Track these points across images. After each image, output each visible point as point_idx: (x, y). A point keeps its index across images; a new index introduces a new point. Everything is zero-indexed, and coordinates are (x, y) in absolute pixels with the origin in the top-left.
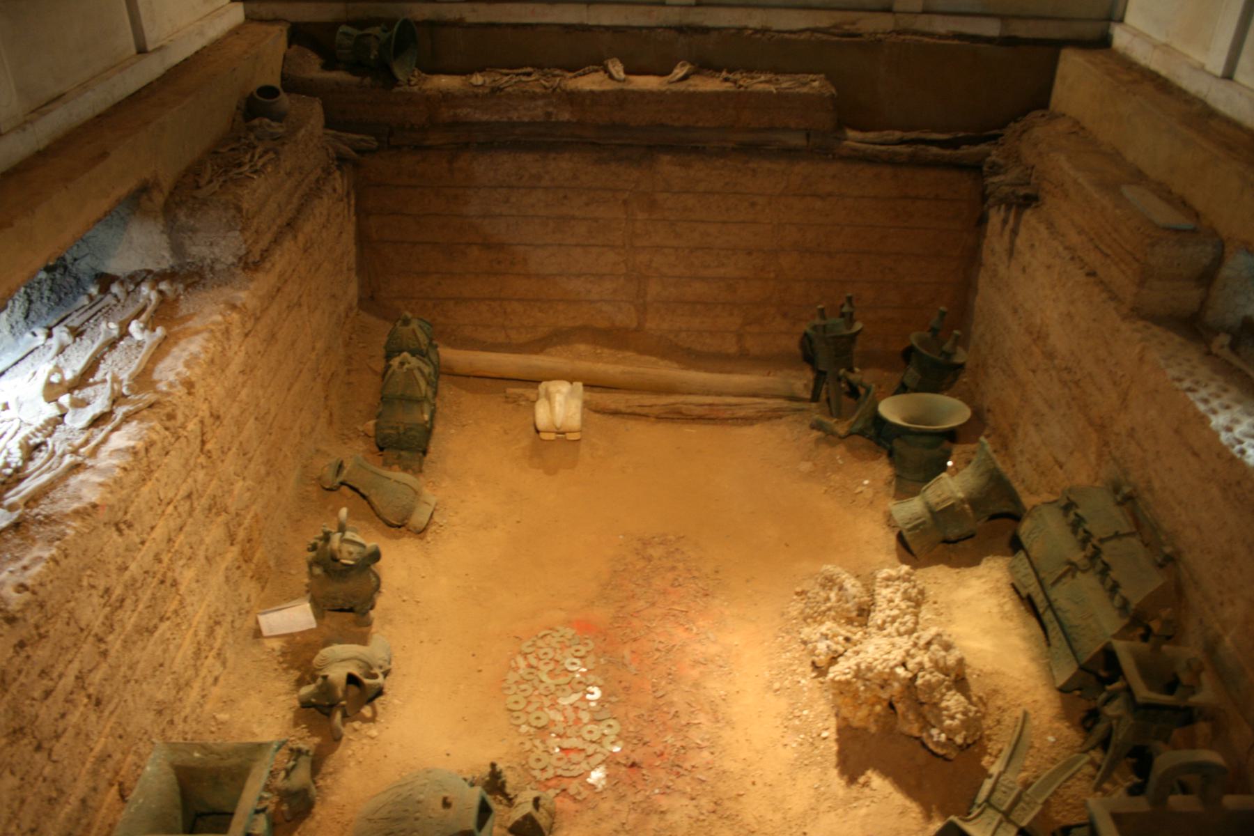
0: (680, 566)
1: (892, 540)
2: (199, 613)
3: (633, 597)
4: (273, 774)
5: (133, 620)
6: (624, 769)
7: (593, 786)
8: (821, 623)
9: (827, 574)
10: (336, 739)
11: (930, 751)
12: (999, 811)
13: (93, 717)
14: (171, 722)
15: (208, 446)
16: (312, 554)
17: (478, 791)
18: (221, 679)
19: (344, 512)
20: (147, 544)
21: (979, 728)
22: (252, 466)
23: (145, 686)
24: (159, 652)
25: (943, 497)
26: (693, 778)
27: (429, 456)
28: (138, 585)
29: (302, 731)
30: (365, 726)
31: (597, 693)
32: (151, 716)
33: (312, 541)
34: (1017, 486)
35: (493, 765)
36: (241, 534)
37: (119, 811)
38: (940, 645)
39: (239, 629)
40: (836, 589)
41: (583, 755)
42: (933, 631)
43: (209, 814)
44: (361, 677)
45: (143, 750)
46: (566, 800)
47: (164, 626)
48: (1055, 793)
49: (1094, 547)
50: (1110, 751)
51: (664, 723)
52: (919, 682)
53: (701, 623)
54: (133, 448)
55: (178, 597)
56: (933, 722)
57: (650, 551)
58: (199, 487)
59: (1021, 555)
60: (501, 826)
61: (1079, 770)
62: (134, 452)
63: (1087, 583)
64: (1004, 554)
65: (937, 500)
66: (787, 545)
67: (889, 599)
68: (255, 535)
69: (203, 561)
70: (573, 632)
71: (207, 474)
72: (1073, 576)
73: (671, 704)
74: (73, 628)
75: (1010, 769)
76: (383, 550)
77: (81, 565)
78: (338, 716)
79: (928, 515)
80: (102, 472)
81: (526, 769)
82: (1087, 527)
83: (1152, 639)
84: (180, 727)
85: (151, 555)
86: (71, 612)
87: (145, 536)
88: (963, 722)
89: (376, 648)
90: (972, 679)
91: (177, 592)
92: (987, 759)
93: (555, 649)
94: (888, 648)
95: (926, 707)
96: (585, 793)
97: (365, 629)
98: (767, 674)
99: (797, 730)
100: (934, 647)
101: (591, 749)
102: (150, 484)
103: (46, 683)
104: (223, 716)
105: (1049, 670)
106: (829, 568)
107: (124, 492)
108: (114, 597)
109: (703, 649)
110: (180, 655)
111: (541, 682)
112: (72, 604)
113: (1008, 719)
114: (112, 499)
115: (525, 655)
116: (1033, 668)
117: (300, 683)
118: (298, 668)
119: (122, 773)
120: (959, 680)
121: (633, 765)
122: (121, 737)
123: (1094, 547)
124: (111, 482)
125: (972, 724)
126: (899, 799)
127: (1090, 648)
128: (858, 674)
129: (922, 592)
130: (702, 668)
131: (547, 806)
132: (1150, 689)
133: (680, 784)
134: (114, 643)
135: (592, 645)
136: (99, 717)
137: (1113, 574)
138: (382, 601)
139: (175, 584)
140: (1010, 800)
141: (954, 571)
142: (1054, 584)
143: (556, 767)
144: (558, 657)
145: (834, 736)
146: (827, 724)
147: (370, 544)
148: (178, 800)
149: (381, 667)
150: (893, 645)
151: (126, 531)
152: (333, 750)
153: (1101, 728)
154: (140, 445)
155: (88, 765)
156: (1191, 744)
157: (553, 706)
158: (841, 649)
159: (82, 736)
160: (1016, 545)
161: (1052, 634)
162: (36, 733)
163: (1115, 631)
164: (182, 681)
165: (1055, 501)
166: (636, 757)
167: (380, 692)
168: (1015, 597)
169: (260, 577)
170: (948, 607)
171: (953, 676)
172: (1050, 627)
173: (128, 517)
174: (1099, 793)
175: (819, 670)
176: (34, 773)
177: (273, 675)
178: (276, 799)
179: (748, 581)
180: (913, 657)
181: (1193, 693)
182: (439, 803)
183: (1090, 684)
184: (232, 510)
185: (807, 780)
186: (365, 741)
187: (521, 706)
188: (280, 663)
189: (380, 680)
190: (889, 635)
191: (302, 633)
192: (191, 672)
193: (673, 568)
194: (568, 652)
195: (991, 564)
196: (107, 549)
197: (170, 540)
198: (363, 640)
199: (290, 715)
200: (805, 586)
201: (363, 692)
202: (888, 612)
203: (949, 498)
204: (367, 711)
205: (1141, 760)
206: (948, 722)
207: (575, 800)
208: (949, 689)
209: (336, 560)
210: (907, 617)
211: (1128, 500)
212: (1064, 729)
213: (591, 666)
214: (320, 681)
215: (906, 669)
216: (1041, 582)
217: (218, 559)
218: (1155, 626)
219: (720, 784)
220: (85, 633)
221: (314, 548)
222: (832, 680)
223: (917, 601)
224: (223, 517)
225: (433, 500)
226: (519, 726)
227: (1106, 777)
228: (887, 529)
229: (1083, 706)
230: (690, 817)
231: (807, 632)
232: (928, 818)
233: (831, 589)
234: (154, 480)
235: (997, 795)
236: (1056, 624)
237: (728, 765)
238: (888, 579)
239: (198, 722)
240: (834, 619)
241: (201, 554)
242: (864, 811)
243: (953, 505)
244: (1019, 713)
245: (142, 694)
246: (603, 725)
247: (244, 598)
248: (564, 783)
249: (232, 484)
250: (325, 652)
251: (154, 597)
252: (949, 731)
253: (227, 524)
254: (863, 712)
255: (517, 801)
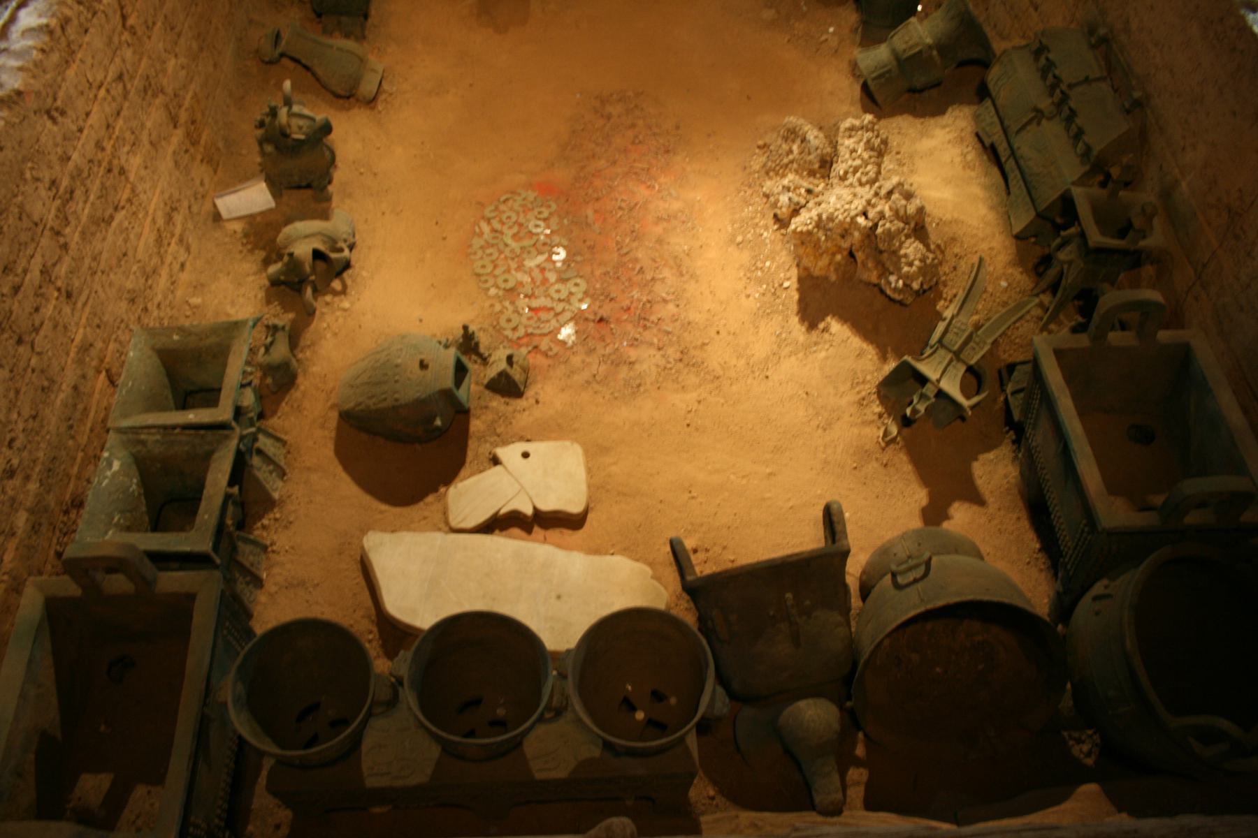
0: (641, 122)
1: (857, 88)
2: (154, 201)
3: (594, 156)
4: (252, 351)
5: (86, 211)
6: (592, 324)
7: (563, 343)
8: (784, 176)
9: (790, 126)
10: (311, 313)
11: (891, 299)
12: (950, 351)
13: (67, 310)
14: (146, 309)
15: (130, 22)
16: (260, 132)
17: (452, 352)
18: (188, 264)
19: (287, 85)
20: (86, 132)
21: (936, 274)
22: (182, 40)
23: (112, 276)
24: (120, 242)
25: (911, 43)
26: (659, 330)
27: (370, 20)
28: (85, 174)
29: (276, 308)
30: (336, 299)
31: (561, 255)
32: (124, 305)
33: (259, 118)
34: (987, 30)
35: (465, 328)
36: (183, 116)
37: (113, 394)
38: (901, 194)
39: (198, 214)
40: (798, 141)
41: (552, 313)
42: (895, 180)
43: (197, 392)
44: (327, 252)
45: (122, 338)
46: (539, 356)
47: (119, 216)
48: (1004, 334)
49: (1062, 92)
50: (1059, 295)
51: (630, 279)
52: (879, 230)
53: (662, 180)
54: (47, 26)
55: (129, 186)
56: (891, 269)
57: (609, 109)
58: (129, 67)
59: (988, 103)
60: (477, 383)
61: (1028, 312)
62: (46, 30)
63: (1052, 130)
64: (970, 103)
65: (904, 46)
66: (749, 98)
67: (852, 150)
68: (199, 116)
69: (148, 146)
70: (536, 194)
71: (134, 52)
72: (1039, 124)
73: (636, 260)
74: (26, 223)
75: (962, 312)
76: (334, 124)
77: (20, 158)
78: (309, 291)
79: (894, 63)
80: (18, 55)
81: (498, 329)
82: (1057, 72)
83: (1110, 185)
84: (155, 313)
85: (92, 144)
86: (21, 207)
87: (81, 123)
88: (920, 268)
89: (338, 223)
90: (931, 227)
91: (127, 179)
92: (942, 303)
93: (518, 213)
94: (849, 198)
95: (885, 255)
96: (556, 349)
97: (325, 205)
98: (730, 229)
99: (760, 281)
100: (895, 196)
101: (559, 307)
102: (74, 66)
103: (11, 279)
104: (196, 301)
105: (1007, 218)
106: (792, 120)
107: (48, 76)
108: (62, 190)
109: (667, 206)
110: (142, 243)
111: (506, 245)
112: (20, 198)
113: (963, 266)
114: (36, 85)
115: (489, 221)
116: (991, 216)
117: (267, 262)
118: (264, 248)
119: (107, 360)
120: (918, 227)
121: (601, 320)
122: (98, 326)
123: (1062, 92)
124: (31, 66)
125: (928, 270)
126: (856, 342)
127: (1049, 195)
128: (819, 224)
129: (885, 142)
130: (665, 224)
131: (521, 362)
132: (1103, 234)
133: (647, 335)
134: (73, 235)
135: (554, 207)
136: (73, 310)
137: (1078, 121)
138: (339, 175)
139: (122, 171)
140: (960, 342)
141: (918, 121)
142: (1018, 132)
143: (526, 327)
144: (522, 220)
145: (795, 286)
146: (788, 275)
147: (319, 117)
148: (166, 380)
149: (345, 241)
150: (855, 195)
151: (60, 119)
152: (309, 325)
153: (1052, 273)
154: (54, 22)
155: (72, 355)
156: (1136, 285)
157: (520, 267)
158: (803, 201)
159: (60, 328)
160: (983, 93)
161: (1012, 183)
162: (14, 328)
163: (1076, 178)
164: (148, 269)
165: (1027, 46)
166: (603, 313)
167: (347, 265)
168: (979, 146)
169: (210, 160)
170: (911, 157)
171: (912, 225)
172: (1011, 177)
173: (59, 103)
174: (1045, 334)
175: (781, 222)
176: (22, 364)
177: (239, 257)
178: (259, 374)
179: (709, 135)
180: (874, 206)
181: (1144, 237)
182: (417, 365)
183: (1044, 232)
184: (169, 90)
185: (770, 328)
186: (338, 313)
187: (489, 269)
188: (243, 245)
189: (346, 253)
190: (851, 185)
191: (262, 213)
192: (155, 260)
193: (633, 126)
194: (530, 215)
195: (957, 113)
196: (43, 139)
197: (108, 126)
198: (325, 215)
199: (261, 294)
200: (768, 139)
201: (330, 267)
202: (850, 162)
203: (917, 45)
204: (336, 285)
205: (1086, 300)
206: (906, 269)
207: (546, 355)
208: (908, 237)
209: (286, 135)
210: (869, 167)
211: (1102, 43)
212: (1017, 274)
213: (555, 227)
214: (286, 259)
215: (867, 218)
216: (1005, 131)
217: (163, 143)
218: (1115, 172)
219: (686, 334)
220: (41, 227)
221: (261, 124)
222: (794, 231)
223: (880, 151)
224: (160, 100)
225: (380, 68)
226: (488, 289)
227: (1054, 318)
228: (851, 79)
229: (1038, 252)
230: (658, 366)
231: (769, 185)
232: (884, 358)
233: (793, 141)
234: (78, 62)
235: (950, 336)
236: (1017, 172)
237: (693, 316)
238: (852, 129)
239: (172, 309)
240: (796, 171)
241: (145, 138)
242: (823, 354)
243: (920, 52)
244: (975, 260)
245: (111, 284)
246: (570, 285)
247: (198, 182)
248: (536, 341)
249: (164, 62)
250: (288, 230)
251: (103, 186)
252: (908, 278)
253: (166, 106)
254: (824, 261)
255: (492, 359)
